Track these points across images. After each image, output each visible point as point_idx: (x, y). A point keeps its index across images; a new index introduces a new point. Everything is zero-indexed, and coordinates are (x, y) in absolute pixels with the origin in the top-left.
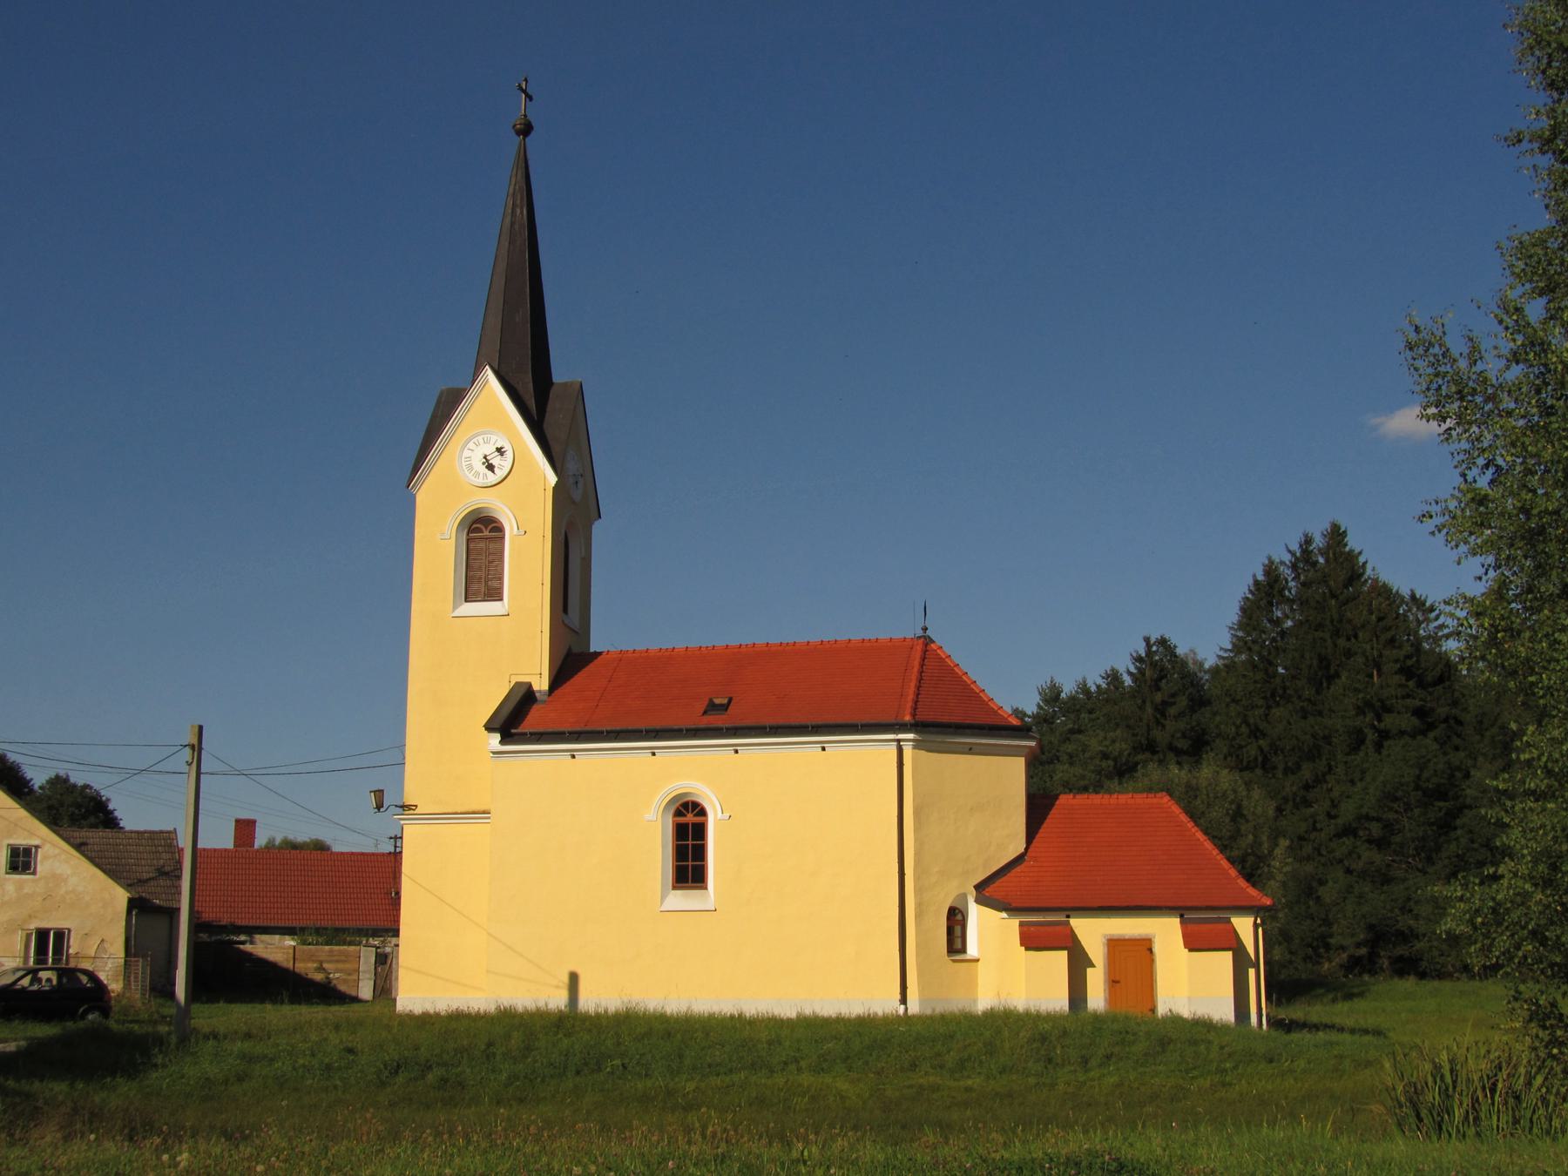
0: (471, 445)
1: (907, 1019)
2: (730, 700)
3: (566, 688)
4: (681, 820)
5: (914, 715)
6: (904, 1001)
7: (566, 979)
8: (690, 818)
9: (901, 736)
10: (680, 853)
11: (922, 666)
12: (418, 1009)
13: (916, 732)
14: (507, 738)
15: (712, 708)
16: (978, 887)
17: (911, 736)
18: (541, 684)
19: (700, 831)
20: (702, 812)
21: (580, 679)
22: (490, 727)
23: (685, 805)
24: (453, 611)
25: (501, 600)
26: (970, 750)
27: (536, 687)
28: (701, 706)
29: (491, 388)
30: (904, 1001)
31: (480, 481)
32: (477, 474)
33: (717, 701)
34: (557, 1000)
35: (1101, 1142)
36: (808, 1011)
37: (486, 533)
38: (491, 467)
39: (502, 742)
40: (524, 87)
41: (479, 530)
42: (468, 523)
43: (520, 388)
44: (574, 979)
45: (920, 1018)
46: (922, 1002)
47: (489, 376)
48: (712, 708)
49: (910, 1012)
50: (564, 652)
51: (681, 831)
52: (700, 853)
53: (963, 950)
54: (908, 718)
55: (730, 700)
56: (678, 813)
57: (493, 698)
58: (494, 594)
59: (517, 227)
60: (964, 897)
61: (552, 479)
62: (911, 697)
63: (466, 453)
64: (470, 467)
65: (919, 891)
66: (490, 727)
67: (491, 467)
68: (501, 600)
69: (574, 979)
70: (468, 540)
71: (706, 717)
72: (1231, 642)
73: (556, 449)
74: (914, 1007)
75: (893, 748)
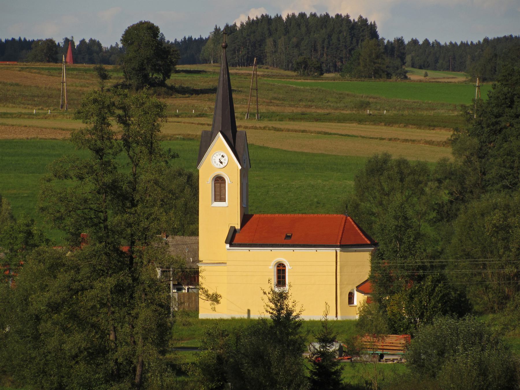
0: (215, 155)
1: (337, 321)
2: (292, 235)
3: (245, 227)
4: (279, 268)
5: (340, 243)
6: (336, 316)
7: (247, 311)
8: (281, 268)
9: (336, 249)
10: (279, 277)
11: (344, 225)
12: (257, 318)
13: (340, 248)
14: (231, 245)
15: (288, 237)
16: (357, 287)
17: (339, 249)
18: (238, 227)
19: (284, 271)
20: (285, 267)
21: (248, 224)
22: (226, 242)
23: (280, 264)
24: (212, 204)
25: (225, 201)
26: (356, 251)
27: (236, 228)
28: (284, 237)
29: (220, 139)
30: (336, 316)
31: (218, 167)
32: (217, 164)
33: (288, 235)
34: (246, 316)
35: (455, 293)
36: (312, 319)
37: (220, 181)
38: (221, 163)
39: (230, 247)
40: (369, 242)
41: (218, 180)
42: (215, 178)
43: (228, 135)
44: (249, 311)
45: (340, 321)
46: (341, 317)
47: (220, 135)
48: (288, 237)
49: (338, 319)
50: (243, 214)
51: (279, 271)
52: (284, 277)
53: (353, 303)
54: (338, 244)
55: (292, 235)
56: (278, 267)
57: (225, 234)
58: (223, 199)
59: (225, 82)
60: (353, 290)
61: (240, 167)
62: (340, 236)
63: (214, 158)
64: (215, 162)
65: (341, 289)
66: (226, 242)
67: (221, 163)
68: (225, 201)
69: (249, 311)
70: (215, 183)
71: (285, 240)
72: (433, 42)
73: (240, 156)
74: (339, 318)
75: (335, 251)
